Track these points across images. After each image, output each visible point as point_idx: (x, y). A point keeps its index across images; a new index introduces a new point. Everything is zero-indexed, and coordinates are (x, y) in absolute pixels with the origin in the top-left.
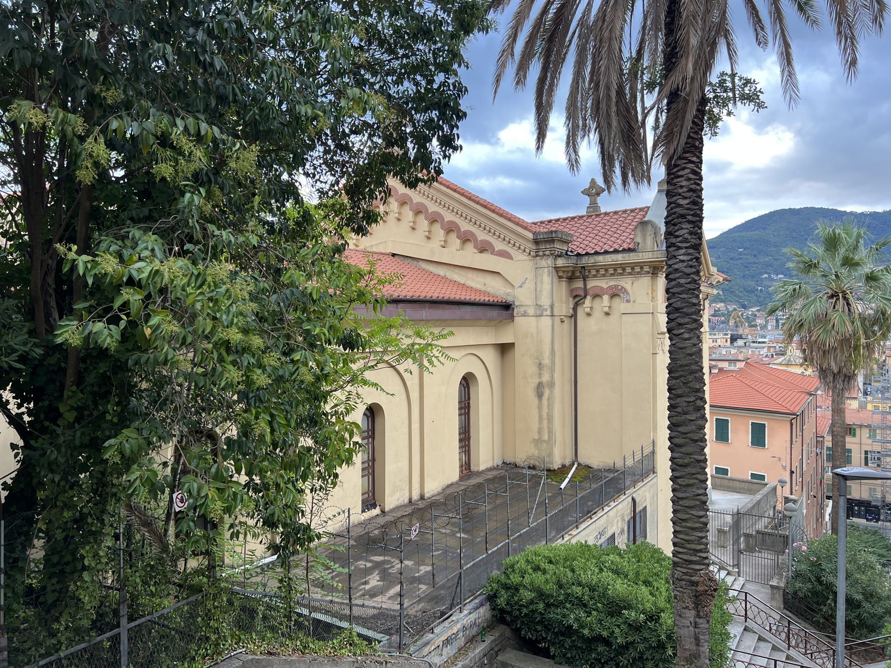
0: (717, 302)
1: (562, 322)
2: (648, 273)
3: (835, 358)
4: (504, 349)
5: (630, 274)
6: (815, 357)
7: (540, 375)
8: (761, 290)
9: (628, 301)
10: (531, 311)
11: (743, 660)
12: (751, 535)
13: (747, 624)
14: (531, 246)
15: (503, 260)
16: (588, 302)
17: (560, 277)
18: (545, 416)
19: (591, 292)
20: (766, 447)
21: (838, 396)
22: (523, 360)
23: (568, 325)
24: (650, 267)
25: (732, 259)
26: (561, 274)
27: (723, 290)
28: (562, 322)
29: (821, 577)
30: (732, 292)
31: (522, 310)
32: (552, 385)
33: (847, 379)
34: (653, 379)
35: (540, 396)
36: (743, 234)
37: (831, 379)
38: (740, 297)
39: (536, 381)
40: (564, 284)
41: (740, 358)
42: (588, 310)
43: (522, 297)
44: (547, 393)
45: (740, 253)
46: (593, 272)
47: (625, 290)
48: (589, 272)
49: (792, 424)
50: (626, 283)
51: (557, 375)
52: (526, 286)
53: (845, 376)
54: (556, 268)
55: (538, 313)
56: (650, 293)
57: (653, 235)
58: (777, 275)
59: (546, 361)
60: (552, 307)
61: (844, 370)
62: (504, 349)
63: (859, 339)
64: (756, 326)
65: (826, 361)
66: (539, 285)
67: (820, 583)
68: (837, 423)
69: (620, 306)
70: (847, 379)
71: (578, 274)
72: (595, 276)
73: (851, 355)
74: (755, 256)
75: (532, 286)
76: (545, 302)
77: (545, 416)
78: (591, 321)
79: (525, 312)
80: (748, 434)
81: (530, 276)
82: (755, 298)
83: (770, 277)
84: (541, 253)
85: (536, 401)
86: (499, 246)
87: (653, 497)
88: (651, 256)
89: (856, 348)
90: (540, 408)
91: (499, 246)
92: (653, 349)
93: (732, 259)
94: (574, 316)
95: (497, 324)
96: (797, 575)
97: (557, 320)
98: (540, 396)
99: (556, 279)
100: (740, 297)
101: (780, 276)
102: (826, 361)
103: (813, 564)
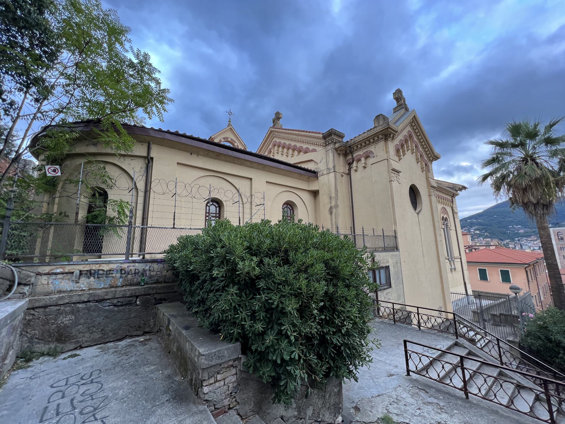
0: (486, 238)
1: (342, 176)
2: (382, 138)
3: (533, 194)
4: (315, 194)
5: (373, 142)
6: (517, 195)
7: (331, 203)
8: (510, 233)
9: (374, 157)
10: (325, 172)
11: (451, 362)
12: (496, 315)
13: (457, 340)
14: (323, 141)
15: (313, 153)
16: (355, 164)
17: (339, 154)
18: (334, 223)
19: (356, 159)
20: (512, 282)
21: (541, 218)
22: (323, 198)
23: (345, 177)
24: (382, 135)
25: (491, 220)
26: (339, 152)
27: (489, 233)
28: (342, 176)
29: (549, 336)
30: (494, 234)
31: (321, 173)
32: (337, 206)
33: (545, 208)
34: (391, 195)
35: (331, 213)
36: (496, 209)
37: (533, 208)
38: (499, 236)
39: (329, 206)
40: (341, 158)
41: (491, 244)
42: (355, 168)
43: (320, 167)
44: (334, 211)
45: (495, 218)
46: (355, 148)
47: (372, 152)
48: (354, 149)
49: (527, 272)
50: (372, 148)
51: (339, 203)
52: (322, 161)
53: (544, 205)
54: (336, 149)
55: (328, 172)
56: (385, 149)
57: (383, 120)
58: (517, 226)
59: (333, 195)
60: (334, 167)
61: (542, 201)
62: (315, 194)
63: (548, 179)
64: (509, 248)
65: (526, 197)
66: (328, 159)
67: (550, 341)
68: (544, 235)
69: (371, 161)
70: (545, 208)
71: (348, 152)
72: (356, 150)
73: (544, 190)
74: (503, 218)
75: (325, 160)
76: (331, 166)
77: (334, 223)
78: (358, 173)
79: (323, 173)
80: (499, 274)
81: (324, 156)
82: (507, 236)
83: (513, 227)
84: (327, 143)
85: (329, 216)
86: (311, 147)
87: (397, 263)
88: (381, 128)
89: (548, 184)
90: (331, 220)
91: (311, 147)
92: (389, 178)
93: (491, 220)
94: (349, 174)
95: (308, 180)
96: (529, 334)
97: (338, 175)
98: (331, 213)
99: (336, 155)
100: (499, 236)
101: (519, 226)
102: (526, 197)
103: (541, 327)
